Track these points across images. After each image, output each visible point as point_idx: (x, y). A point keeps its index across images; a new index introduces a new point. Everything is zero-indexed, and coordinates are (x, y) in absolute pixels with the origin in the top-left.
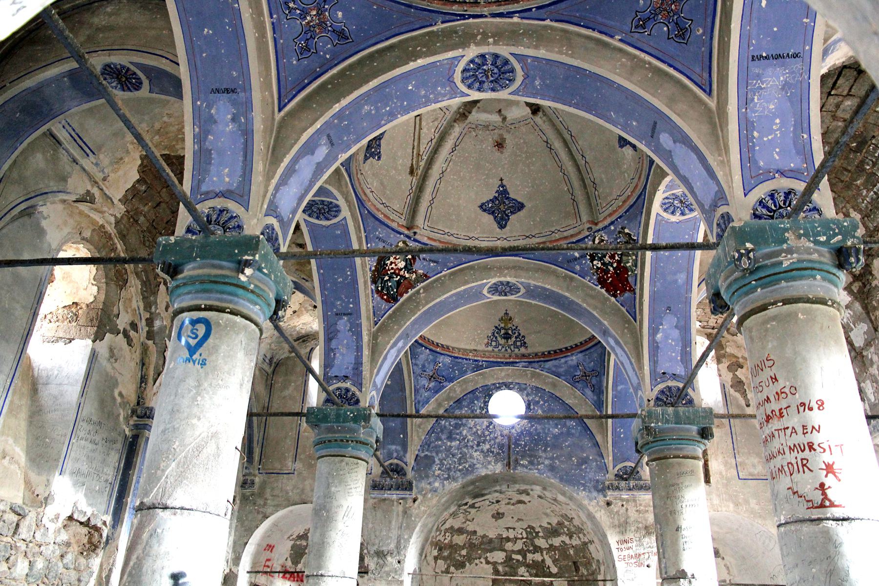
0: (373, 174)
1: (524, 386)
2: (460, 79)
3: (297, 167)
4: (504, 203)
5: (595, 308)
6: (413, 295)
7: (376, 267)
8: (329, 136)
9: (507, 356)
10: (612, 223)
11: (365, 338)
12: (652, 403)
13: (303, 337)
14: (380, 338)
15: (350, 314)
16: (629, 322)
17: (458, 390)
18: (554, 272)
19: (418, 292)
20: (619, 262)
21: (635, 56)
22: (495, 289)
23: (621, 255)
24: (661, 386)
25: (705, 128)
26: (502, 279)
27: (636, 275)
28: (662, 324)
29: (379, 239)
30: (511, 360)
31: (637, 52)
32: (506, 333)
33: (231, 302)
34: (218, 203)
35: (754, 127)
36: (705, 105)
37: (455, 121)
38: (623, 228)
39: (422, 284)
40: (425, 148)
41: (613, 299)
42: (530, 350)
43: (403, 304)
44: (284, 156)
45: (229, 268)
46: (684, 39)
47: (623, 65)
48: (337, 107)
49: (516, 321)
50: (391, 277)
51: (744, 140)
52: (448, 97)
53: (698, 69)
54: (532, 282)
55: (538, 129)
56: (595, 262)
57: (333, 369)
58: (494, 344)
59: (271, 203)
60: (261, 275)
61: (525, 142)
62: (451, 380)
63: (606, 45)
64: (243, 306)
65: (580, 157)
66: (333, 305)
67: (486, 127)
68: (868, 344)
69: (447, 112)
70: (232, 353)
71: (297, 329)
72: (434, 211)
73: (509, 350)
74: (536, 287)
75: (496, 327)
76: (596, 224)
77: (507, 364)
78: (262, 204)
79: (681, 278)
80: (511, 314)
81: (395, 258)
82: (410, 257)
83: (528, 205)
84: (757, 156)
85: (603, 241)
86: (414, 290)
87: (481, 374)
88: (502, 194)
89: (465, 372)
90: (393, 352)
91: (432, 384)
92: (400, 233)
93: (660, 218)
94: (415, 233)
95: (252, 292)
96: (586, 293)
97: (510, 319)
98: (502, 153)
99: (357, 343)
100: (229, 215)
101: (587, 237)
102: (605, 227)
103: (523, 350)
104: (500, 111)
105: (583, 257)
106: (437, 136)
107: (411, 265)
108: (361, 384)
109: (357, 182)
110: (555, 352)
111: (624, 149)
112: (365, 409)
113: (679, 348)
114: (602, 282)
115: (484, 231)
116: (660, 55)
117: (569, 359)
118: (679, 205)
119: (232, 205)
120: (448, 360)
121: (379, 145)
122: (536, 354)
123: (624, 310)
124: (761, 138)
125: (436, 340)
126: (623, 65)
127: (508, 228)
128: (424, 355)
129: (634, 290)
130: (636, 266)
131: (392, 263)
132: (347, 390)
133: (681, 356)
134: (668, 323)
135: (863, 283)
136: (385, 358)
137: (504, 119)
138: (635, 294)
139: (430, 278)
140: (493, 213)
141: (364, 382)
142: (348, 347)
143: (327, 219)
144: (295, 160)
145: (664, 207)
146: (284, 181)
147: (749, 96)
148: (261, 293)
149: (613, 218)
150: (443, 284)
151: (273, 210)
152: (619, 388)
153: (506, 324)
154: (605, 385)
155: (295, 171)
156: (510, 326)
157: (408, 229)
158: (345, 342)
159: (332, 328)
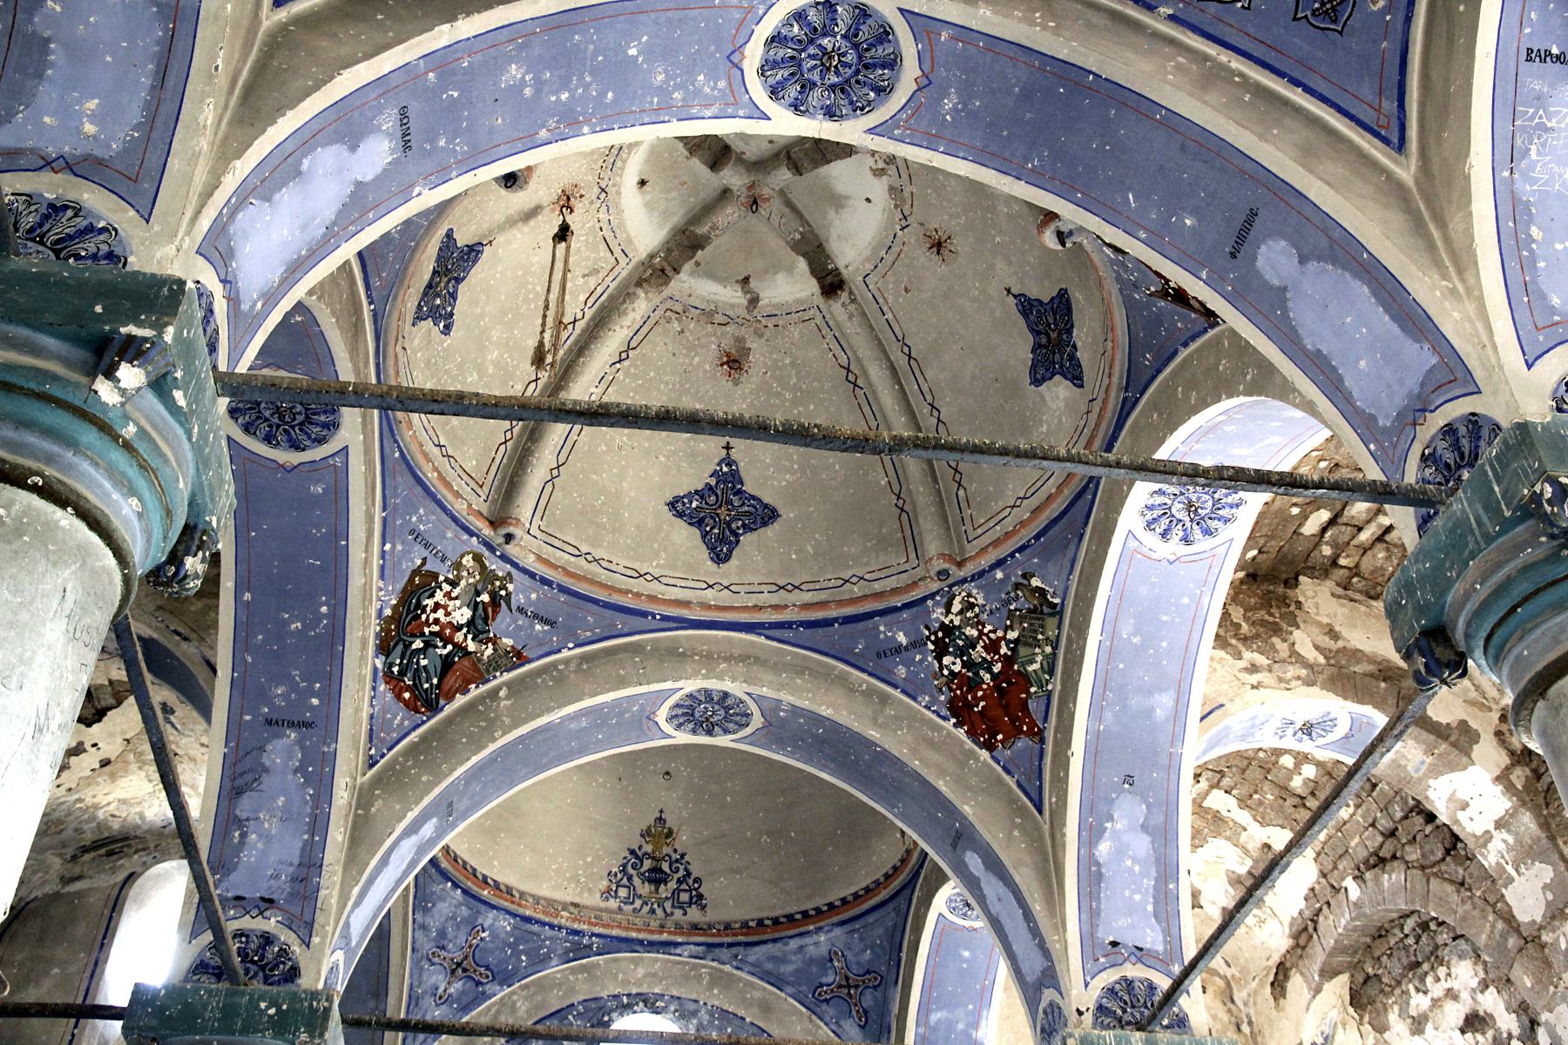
0: (428, 363)
1: (692, 1007)
2: (757, 64)
3: (306, 163)
4: (730, 502)
5: (942, 773)
6: (481, 699)
7: (395, 608)
8: (404, 113)
9: (654, 924)
10: (1000, 563)
11: (342, 796)
12: (1088, 1018)
13: (113, 840)
14: (379, 804)
15: (308, 725)
16: (1022, 811)
17: (522, 1006)
18: (842, 679)
19: (493, 694)
20: (1008, 661)
21: (1206, 58)
22: (691, 713)
23: (1016, 641)
24: (1109, 977)
25: (1397, 219)
26: (714, 684)
27: (1049, 694)
28: (1111, 818)
29: (417, 535)
30: (665, 937)
31: (1211, 49)
32: (656, 870)
33: (50, 459)
34: (50, 187)
35: (1530, 214)
36: (1389, 175)
37: (639, 284)
38: (1027, 576)
39: (507, 676)
40: (577, 306)
41: (984, 754)
42: (712, 916)
43: (449, 720)
44: (281, 110)
45: (59, 358)
46: (1335, 22)
47: (1179, 67)
48: (442, 36)
49: (683, 840)
50: (428, 645)
51: (1509, 242)
52: (714, 110)
53: (1367, 91)
54: (787, 697)
55: (829, 336)
56: (947, 660)
57: (234, 877)
58: (623, 892)
59: (220, 228)
60: (161, 408)
61: (792, 364)
62: (506, 979)
63: (1137, 26)
64: (92, 484)
65: (927, 410)
66: (263, 696)
67: (708, 315)
68: (1555, 914)
69: (623, 261)
70: (24, 616)
71: (101, 814)
72: (558, 494)
73: (659, 912)
74: (795, 711)
75: (632, 852)
76: (960, 565)
77: (652, 946)
78: (198, 212)
79: (1163, 703)
80: (671, 822)
81: (448, 595)
82: (485, 598)
83: (787, 513)
84: (1544, 283)
85: (972, 606)
86: (483, 688)
87: (583, 969)
88: (725, 482)
89: (540, 962)
90: (408, 847)
91: (458, 986)
92: (472, 534)
93: (1132, 544)
94: (509, 538)
95: (127, 446)
96: (918, 734)
97: (670, 833)
98: (736, 383)
99: (316, 806)
100: (81, 223)
101: (932, 596)
102: (981, 574)
103: (694, 914)
104: (746, 280)
105: (917, 644)
106: (589, 313)
107: (486, 620)
108: (310, 925)
109: (391, 362)
110: (776, 921)
111: (1043, 388)
112: (314, 995)
113: (1149, 883)
114: (960, 711)
115: (673, 563)
116: (1270, 57)
117: (808, 940)
118: (1182, 515)
119: (97, 201)
120: (506, 924)
121: (454, 296)
122: (728, 926)
123: (1011, 782)
124: (1549, 241)
125: (482, 869)
126: (1179, 67)
127: (734, 562)
128: (449, 902)
129: (1041, 732)
130: (1051, 672)
131: (437, 606)
132: (267, 939)
133: (1156, 903)
134: (1127, 815)
135: (1535, 771)
136: (384, 862)
137: (754, 301)
138: (1042, 741)
139: (529, 661)
140: (699, 523)
141: (320, 918)
142: (287, 817)
143: (296, 446)
144: (307, 139)
145: (1149, 517)
146: (264, 185)
147: (1518, 142)
148: (154, 462)
149: (1002, 552)
150: (560, 680)
151: (218, 249)
152: (934, 1018)
153: (657, 847)
154: (896, 1010)
155: (300, 173)
156: (666, 850)
157: (494, 524)
158: (281, 801)
159: (247, 763)
